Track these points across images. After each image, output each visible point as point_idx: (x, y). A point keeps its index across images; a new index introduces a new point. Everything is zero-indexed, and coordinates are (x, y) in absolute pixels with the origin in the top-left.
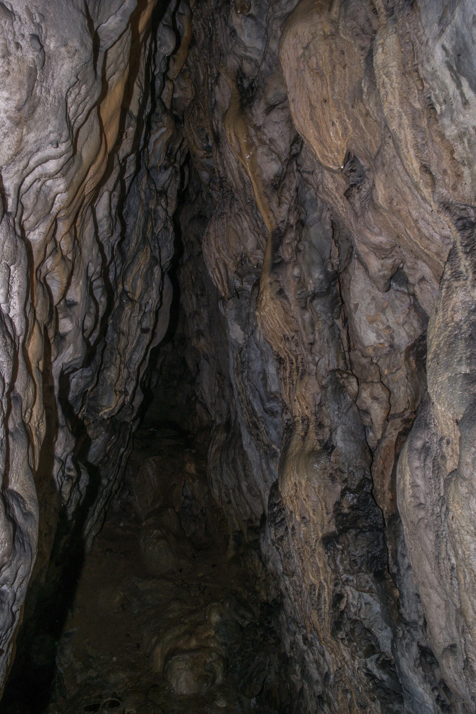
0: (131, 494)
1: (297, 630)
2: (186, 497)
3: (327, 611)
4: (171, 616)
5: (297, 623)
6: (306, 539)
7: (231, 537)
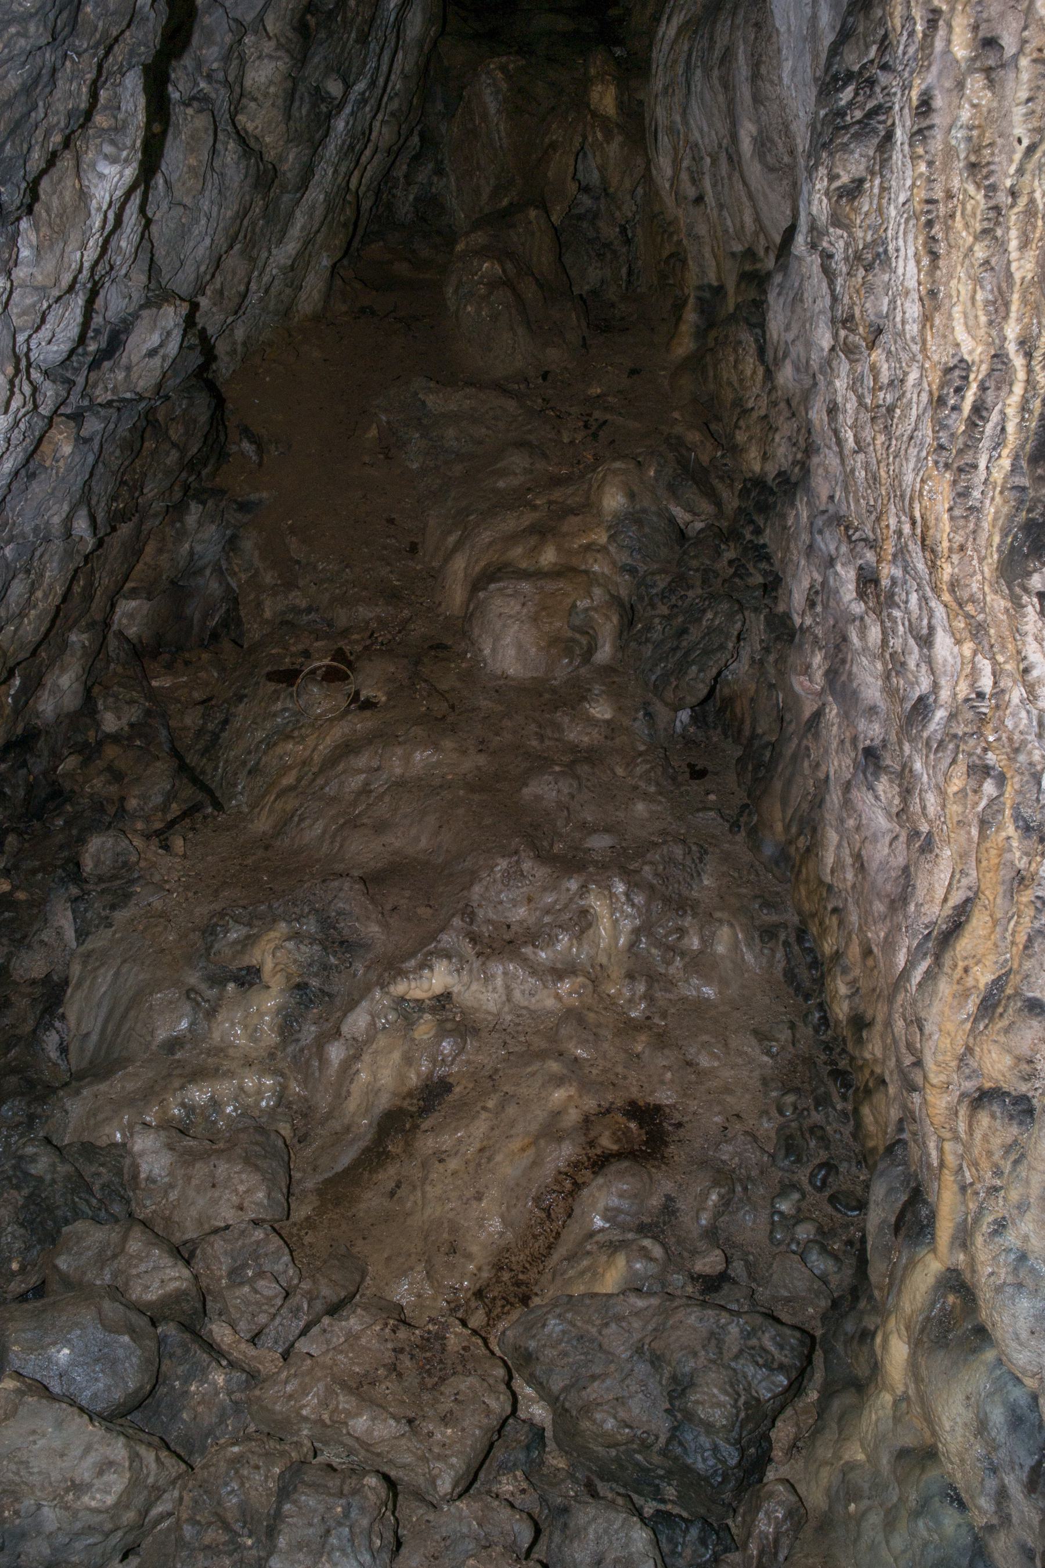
0: (439, 172)
1: (844, 549)
2: (585, 189)
3: (998, 476)
4: (501, 484)
5: (847, 528)
6: (977, 150)
7: (692, 301)
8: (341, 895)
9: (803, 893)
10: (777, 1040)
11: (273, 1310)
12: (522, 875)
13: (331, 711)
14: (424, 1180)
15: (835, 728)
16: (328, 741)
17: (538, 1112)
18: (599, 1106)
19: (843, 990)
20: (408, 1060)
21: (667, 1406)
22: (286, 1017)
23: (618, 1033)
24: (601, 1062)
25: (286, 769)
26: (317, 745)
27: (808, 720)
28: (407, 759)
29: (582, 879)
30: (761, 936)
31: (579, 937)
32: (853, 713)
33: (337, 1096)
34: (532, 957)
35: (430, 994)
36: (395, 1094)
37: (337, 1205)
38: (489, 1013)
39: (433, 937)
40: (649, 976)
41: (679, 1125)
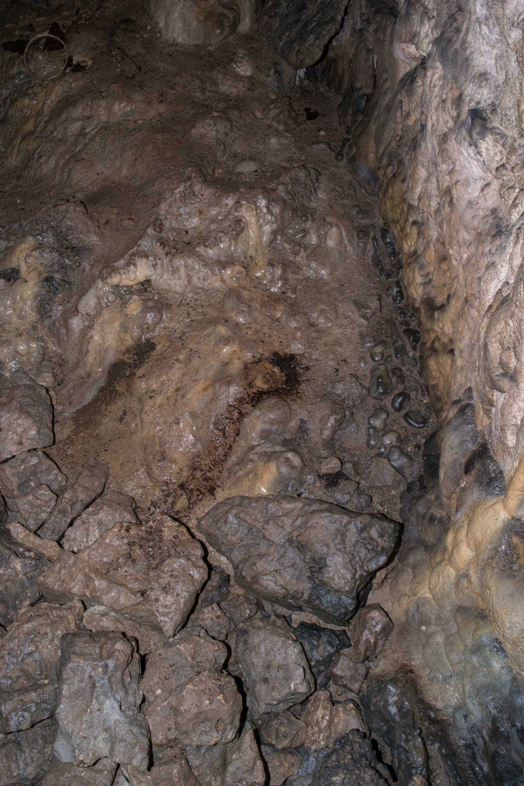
8: (68, 215)
9: (389, 206)
10: (369, 308)
11: (49, 510)
12: (194, 195)
13: (53, 73)
14: (141, 411)
15: (437, 89)
16: (53, 97)
17: (213, 363)
18: (254, 357)
19: (419, 279)
20: (124, 328)
21: (309, 574)
22: (40, 301)
23: (264, 305)
24: (253, 325)
25: (25, 119)
26: (46, 100)
27: (402, 80)
28: (109, 108)
29: (236, 197)
30: (358, 235)
31: (235, 239)
32: (463, 78)
33: (81, 352)
34: (204, 254)
35: (136, 282)
36: (118, 351)
37: (86, 428)
38: (177, 293)
39: (135, 242)
40: (284, 264)
41: (307, 368)
